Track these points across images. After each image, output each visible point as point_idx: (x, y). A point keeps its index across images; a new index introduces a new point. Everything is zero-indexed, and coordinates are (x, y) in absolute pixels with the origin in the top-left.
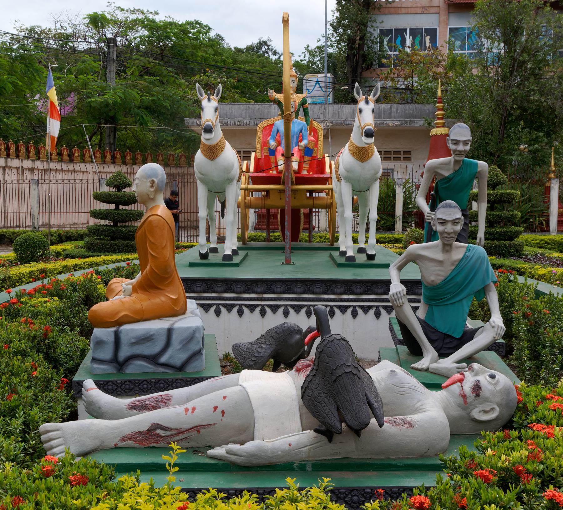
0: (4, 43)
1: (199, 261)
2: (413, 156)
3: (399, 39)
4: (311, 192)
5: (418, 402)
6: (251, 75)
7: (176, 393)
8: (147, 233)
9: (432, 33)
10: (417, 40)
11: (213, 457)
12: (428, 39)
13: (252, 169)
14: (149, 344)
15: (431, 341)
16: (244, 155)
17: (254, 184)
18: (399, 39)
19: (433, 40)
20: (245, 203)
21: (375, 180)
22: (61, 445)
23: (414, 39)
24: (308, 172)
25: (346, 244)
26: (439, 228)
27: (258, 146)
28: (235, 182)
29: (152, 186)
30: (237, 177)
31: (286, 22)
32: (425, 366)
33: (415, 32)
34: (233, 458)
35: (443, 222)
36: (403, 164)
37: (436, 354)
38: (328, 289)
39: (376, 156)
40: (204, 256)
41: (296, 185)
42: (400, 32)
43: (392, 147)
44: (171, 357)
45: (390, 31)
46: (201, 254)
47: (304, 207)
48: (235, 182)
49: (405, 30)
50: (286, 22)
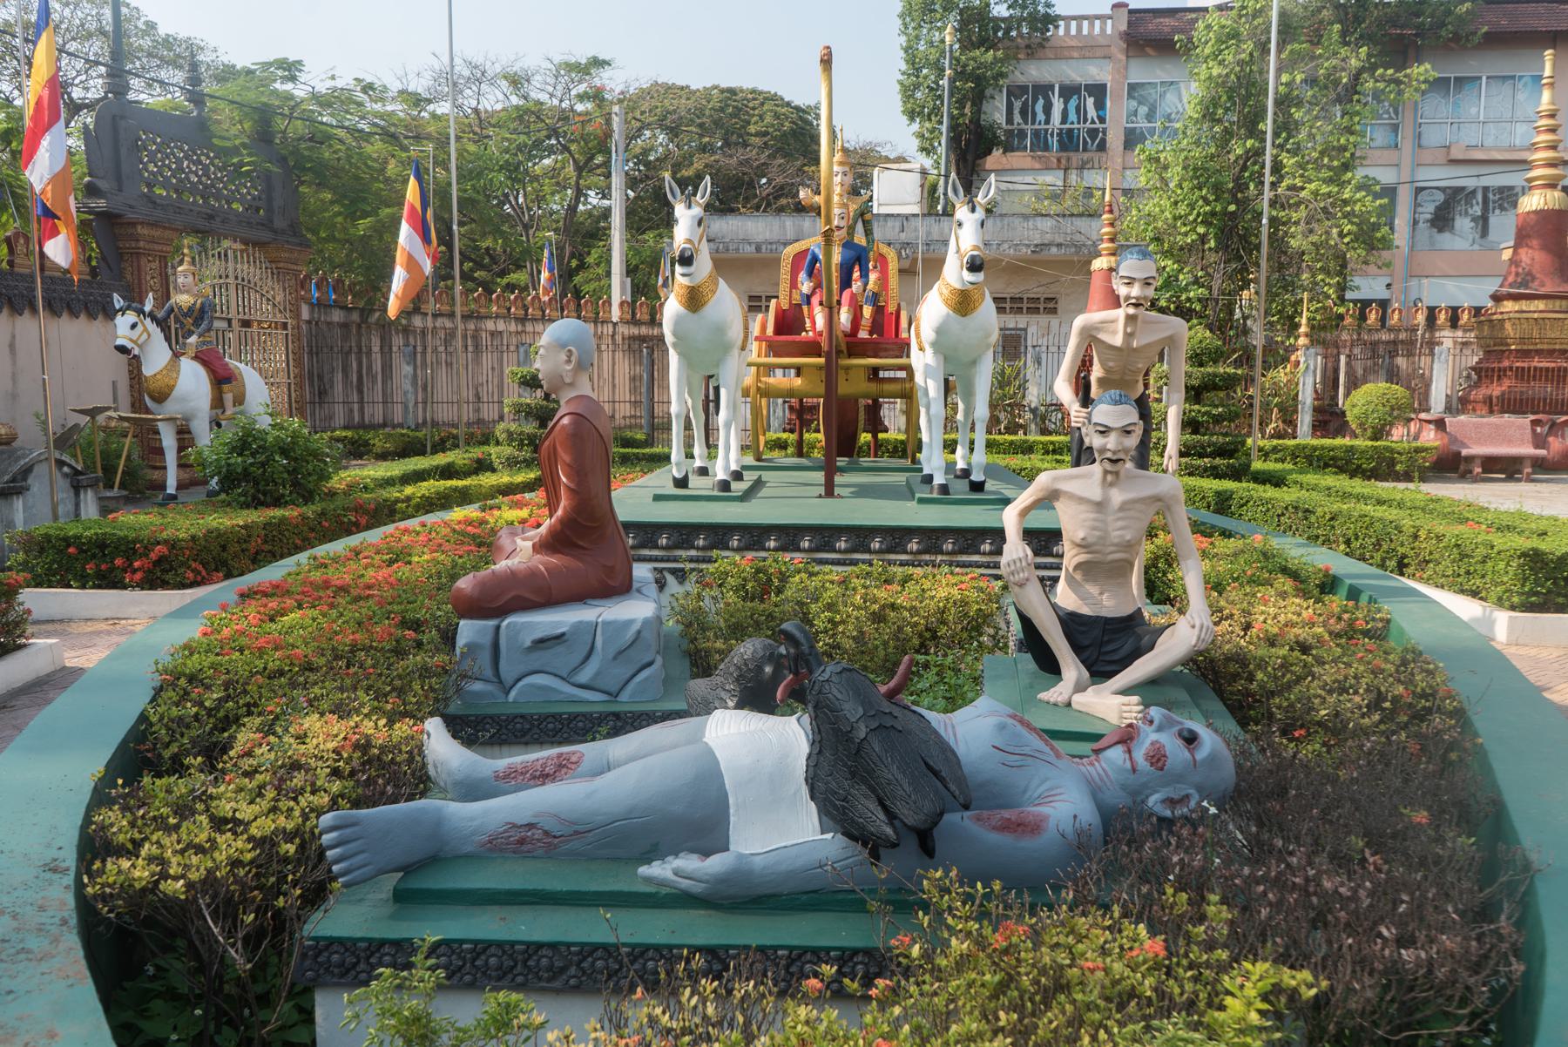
0: (6, 22)
1: (672, 490)
2: (1061, 306)
3: (1041, 102)
4: (875, 370)
5: (1043, 782)
6: (754, 152)
7: (590, 751)
8: (559, 449)
9: (1098, 91)
10: (1073, 103)
11: (649, 880)
12: (1090, 101)
13: (770, 331)
14: (560, 649)
15: (1077, 648)
16: (755, 304)
17: (776, 355)
18: (1041, 102)
19: (1100, 105)
20: (758, 389)
21: (988, 347)
22: (362, 852)
23: (1066, 103)
24: (871, 333)
25: (932, 461)
26: (1096, 441)
27: (784, 288)
28: (736, 352)
29: (569, 361)
30: (740, 343)
31: (827, 62)
32: (1061, 699)
33: (1068, 91)
34: (685, 884)
35: (1105, 431)
36: (1043, 319)
37: (1086, 674)
38: (897, 545)
39: (988, 307)
40: (682, 483)
41: (850, 356)
42: (1043, 90)
43: (1010, 291)
44: (598, 674)
45: (1023, 89)
46: (675, 479)
47: (866, 396)
48: (736, 352)
49: (1052, 87)
50: (827, 62)
